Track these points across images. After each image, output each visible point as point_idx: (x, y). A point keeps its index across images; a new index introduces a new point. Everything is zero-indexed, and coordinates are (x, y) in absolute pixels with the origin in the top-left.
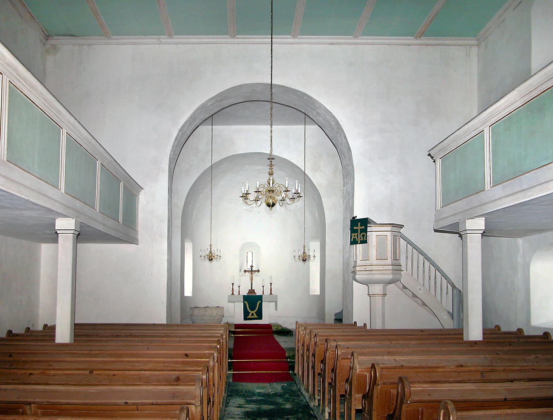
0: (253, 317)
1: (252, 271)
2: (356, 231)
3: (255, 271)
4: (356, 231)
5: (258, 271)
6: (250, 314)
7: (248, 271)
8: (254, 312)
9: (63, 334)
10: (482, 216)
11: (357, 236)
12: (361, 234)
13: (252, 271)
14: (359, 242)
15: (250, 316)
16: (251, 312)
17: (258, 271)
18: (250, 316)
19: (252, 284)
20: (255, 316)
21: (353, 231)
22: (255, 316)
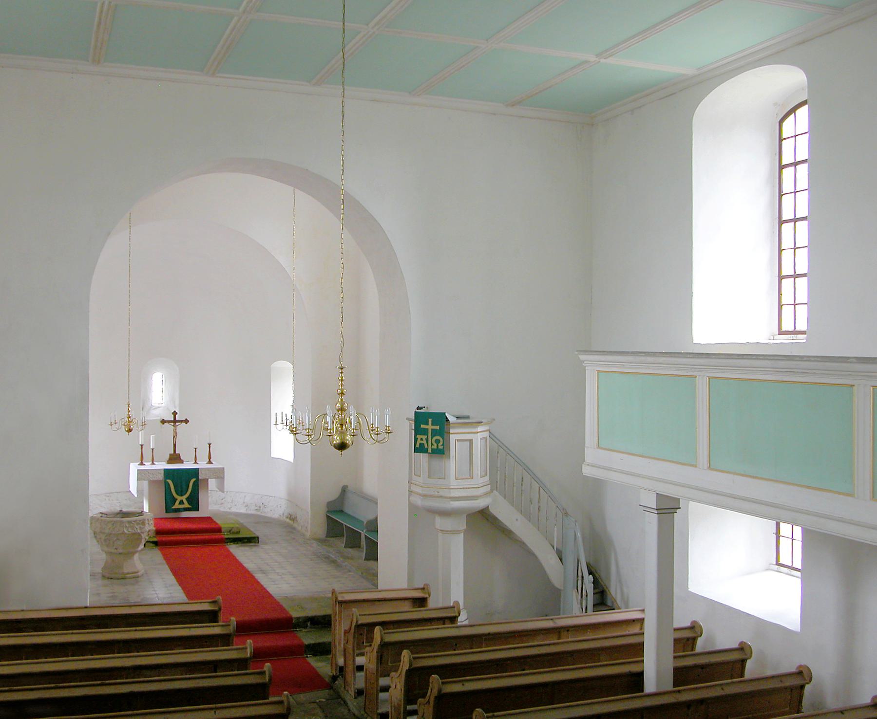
0: (182, 506)
1: (175, 421)
2: (425, 432)
3: (181, 421)
4: (425, 432)
5: (186, 421)
6: (177, 502)
7: (169, 422)
8: (184, 498)
9: (655, 669)
10: (354, 674)
11: (427, 440)
12: (434, 438)
13: (175, 421)
14: (430, 451)
15: (177, 505)
16: (179, 498)
17: (186, 421)
18: (177, 505)
19: (175, 445)
20: (186, 505)
21: (418, 431)
22: (186, 505)
